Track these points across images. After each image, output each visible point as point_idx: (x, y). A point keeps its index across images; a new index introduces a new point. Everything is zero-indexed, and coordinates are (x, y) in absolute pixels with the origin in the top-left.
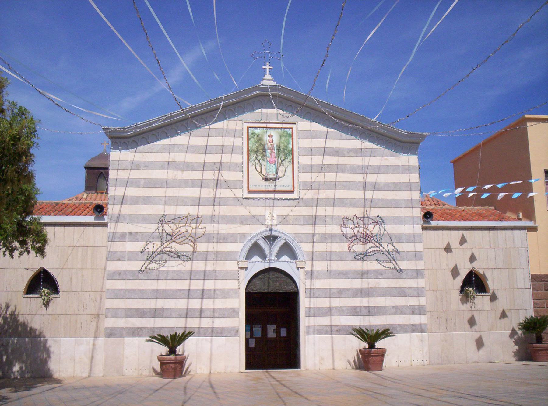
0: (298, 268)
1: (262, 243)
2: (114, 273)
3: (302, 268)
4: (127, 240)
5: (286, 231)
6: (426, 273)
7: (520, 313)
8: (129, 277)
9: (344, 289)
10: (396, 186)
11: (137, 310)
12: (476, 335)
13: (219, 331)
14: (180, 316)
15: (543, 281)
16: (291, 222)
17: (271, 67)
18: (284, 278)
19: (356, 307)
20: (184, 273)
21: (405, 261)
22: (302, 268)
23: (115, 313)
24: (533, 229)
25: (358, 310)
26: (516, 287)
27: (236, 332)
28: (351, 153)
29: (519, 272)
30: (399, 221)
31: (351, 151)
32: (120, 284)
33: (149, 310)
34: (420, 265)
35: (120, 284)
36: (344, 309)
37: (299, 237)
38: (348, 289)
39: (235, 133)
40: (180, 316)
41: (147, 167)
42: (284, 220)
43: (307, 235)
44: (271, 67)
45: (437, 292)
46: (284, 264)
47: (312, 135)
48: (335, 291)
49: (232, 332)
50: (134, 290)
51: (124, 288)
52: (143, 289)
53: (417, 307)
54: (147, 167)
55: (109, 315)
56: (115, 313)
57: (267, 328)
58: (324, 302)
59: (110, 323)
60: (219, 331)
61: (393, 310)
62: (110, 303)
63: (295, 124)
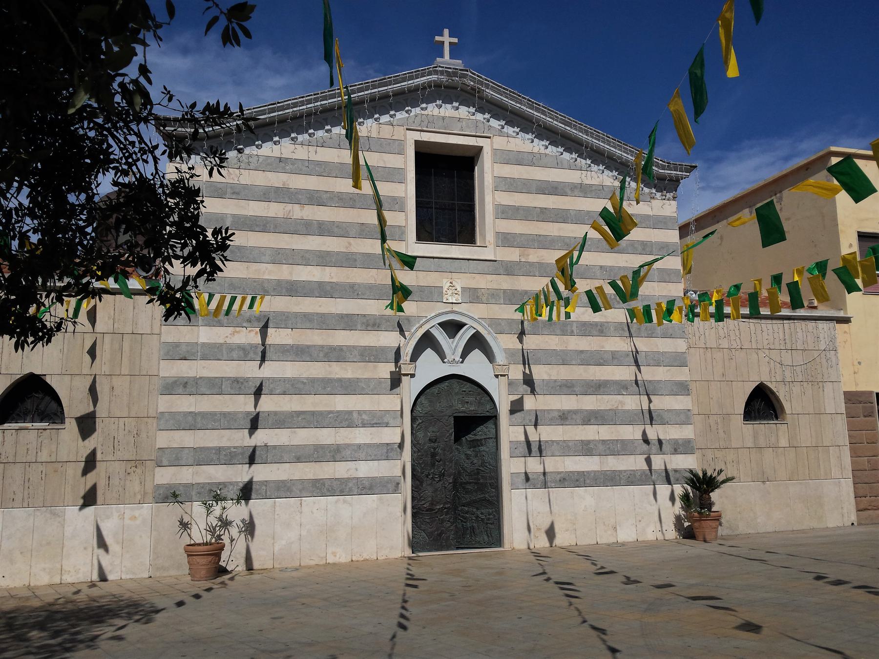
0: (497, 376)
1: (440, 336)
2: (175, 382)
3: (504, 375)
4: (200, 322)
5: (476, 317)
6: (692, 386)
8: (203, 390)
9: (569, 411)
11: (219, 450)
12: (91, 478)
14: (298, 459)
16: (484, 299)
17: (455, 40)
19: (589, 442)
20: (304, 383)
21: (661, 368)
22: (504, 375)
23: (175, 458)
24: (846, 320)
25: (592, 446)
27: (394, 487)
28: (576, 192)
31: (575, 187)
32: (185, 404)
33: (240, 450)
34: (681, 375)
37: (497, 325)
38: (575, 412)
40: (298, 459)
41: (238, 194)
42: (473, 295)
43: (510, 322)
44: (455, 40)
46: (476, 367)
47: (519, 159)
48: (556, 414)
49: (389, 486)
50: (213, 414)
51: (192, 409)
52: (229, 413)
53: (680, 442)
54: (238, 194)
55: (165, 463)
56: (175, 458)
61: (601, 447)
62: (166, 439)
63: (489, 138)
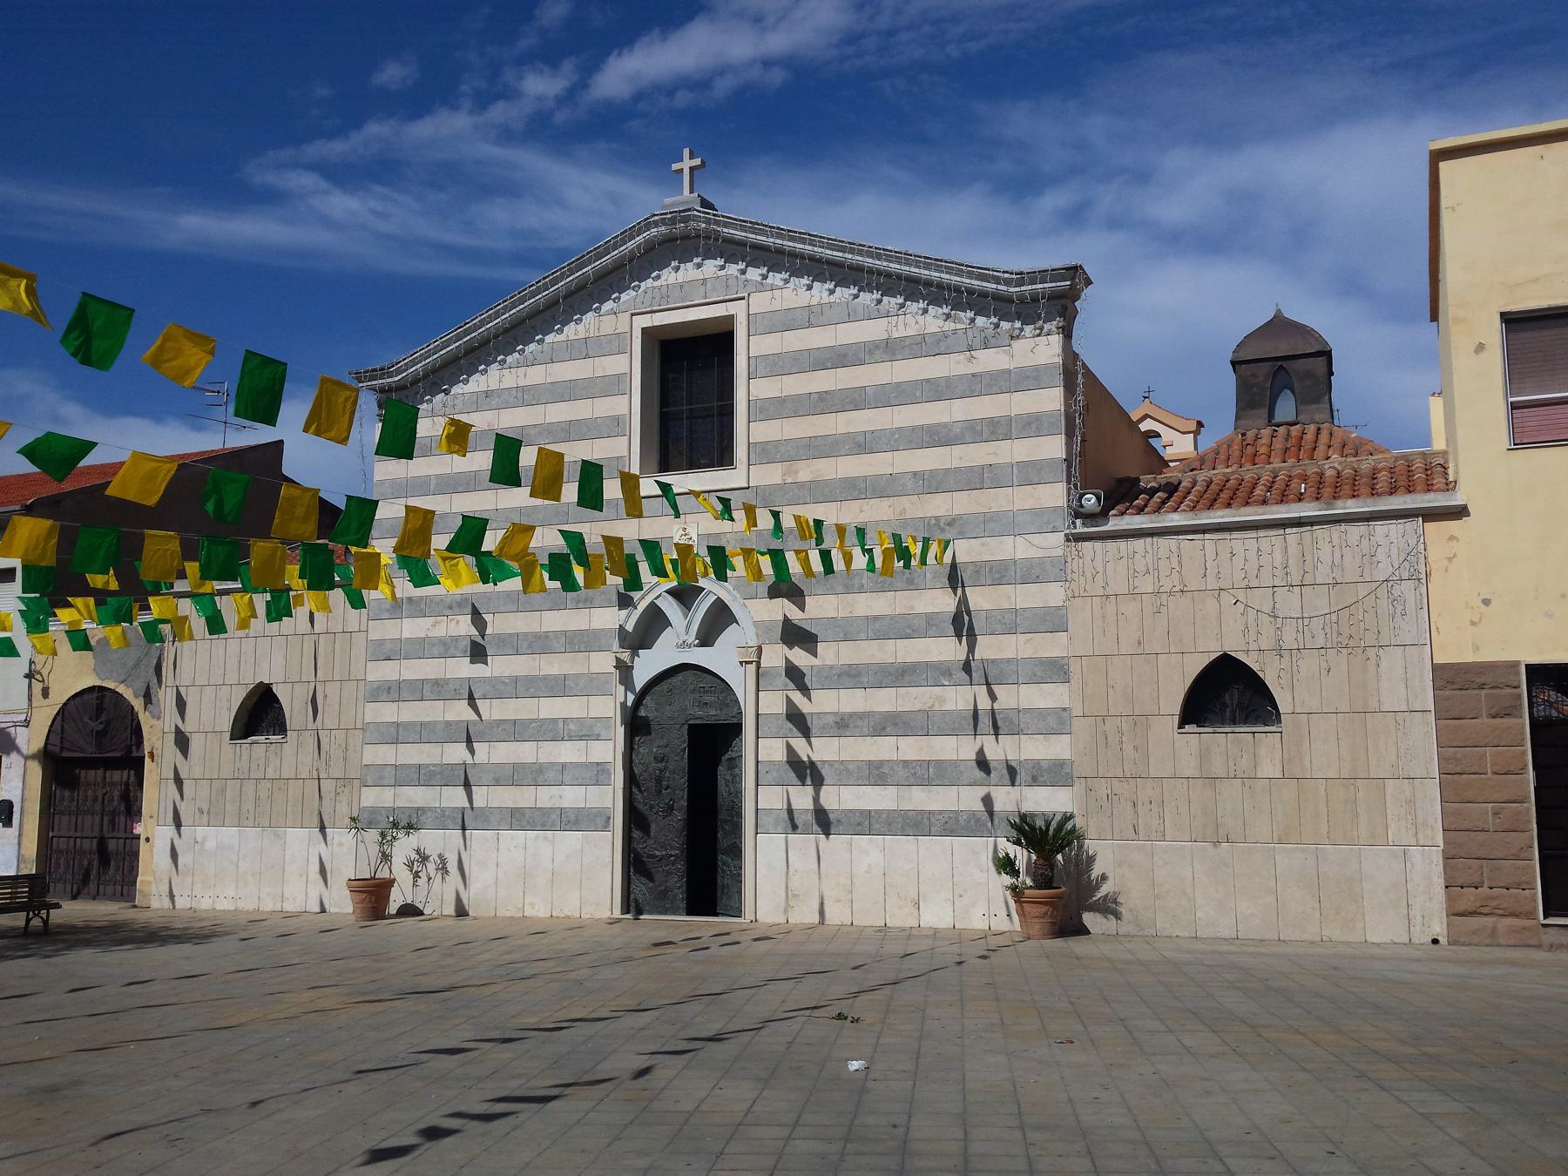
6: (1074, 667)
7: (1389, 791)
9: (851, 715)
10: (997, 429)
13: (572, 818)
15: (1482, 687)
17: (686, 152)
18: (676, 680)
19: (881, 763)
24: (1460, 512)
26: (1373, 706)
27: (606, 825)
28: (878, 355)
29: (1392, 661)
30: (1004, 525)
32: (387, 713)
35: (387, 713)
36: (851, 767)
39: (615, 344)
45: (1109, 720)
48: (831, 719)
53: (1045, 765)
57: (59, 926)
58: (568, 752)
59: (372, 797)
60: (572, 818)
